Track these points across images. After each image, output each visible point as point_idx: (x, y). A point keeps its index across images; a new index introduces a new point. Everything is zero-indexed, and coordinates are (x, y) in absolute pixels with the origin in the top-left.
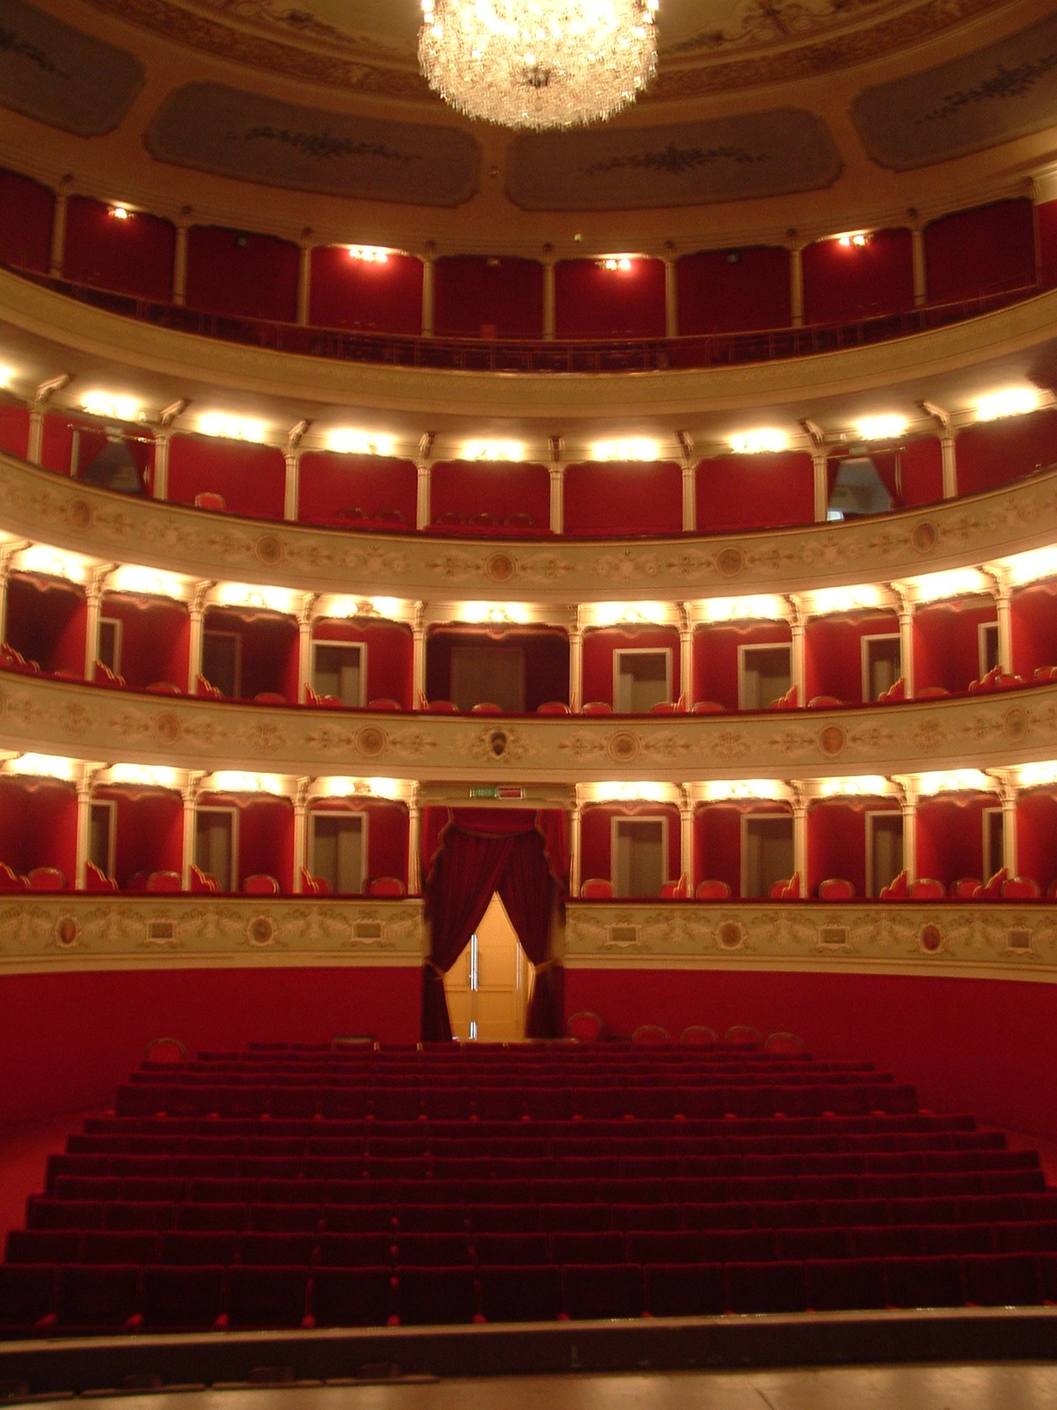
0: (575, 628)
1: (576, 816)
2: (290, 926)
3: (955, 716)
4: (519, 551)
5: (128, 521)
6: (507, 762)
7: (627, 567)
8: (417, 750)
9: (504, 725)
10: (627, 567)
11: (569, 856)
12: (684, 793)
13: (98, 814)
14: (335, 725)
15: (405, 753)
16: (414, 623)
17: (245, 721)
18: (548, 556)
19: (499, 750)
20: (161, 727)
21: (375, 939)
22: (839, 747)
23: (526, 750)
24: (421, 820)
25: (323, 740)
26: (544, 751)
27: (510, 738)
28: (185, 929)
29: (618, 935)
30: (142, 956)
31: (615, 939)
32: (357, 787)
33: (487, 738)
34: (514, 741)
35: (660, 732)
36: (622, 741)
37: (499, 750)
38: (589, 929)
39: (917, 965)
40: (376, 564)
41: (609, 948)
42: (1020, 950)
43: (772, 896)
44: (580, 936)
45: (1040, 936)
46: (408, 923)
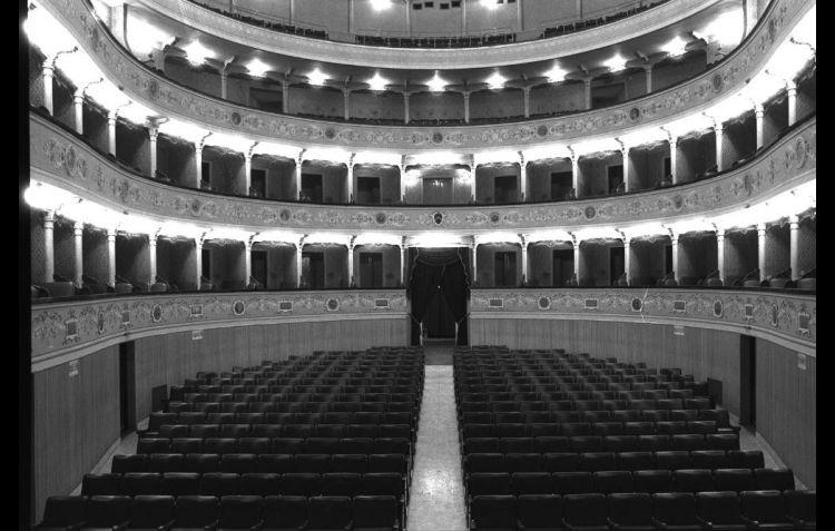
1: (475, 250)
3: (648, 199)
4: (502, 211)
5: (261, 121)
7: (495, 136)
10: (495, 136)
12: (523, 239)
13: (205, 253)
15: (396, 224)
17: (322, 212)
18: (459, 132)
19: (438, 221)
20: (282, 215)
22: (593, 216)
28: (296, 304)
29: (493, 303)
30: (62, 351)
31: (329, 389)
35: (458, 130)
37: (438, 221)
38: (480, 300)
40: (380, 138)
42: (680, 311)
44: (476, 303)
45: (689, 304)
46: (399, 299)
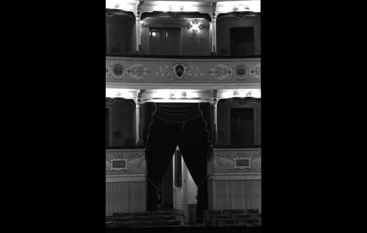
0: (214, 14)
2: (132, 162)
6: (184, 80)
8: (141, 74)
9: (182, 62)
11: (136, 126)
14: (222, 65)
15: (134, 76)
16: (135, 12)
19: (180, 74)
21: (122, 168)
23: (193, 74)
24: (140, 108)
25: (216, 72)
26: (202, 74)
27: (185, 68)
29: (239, 163)
32: (235, 94)
33: (174, 69)
34: (187, 70)
36: (240, 69)
37: (180, 74)
38: (225, 161)
39: (114, 177)
41: (236, 170)
43: (256, 144)
